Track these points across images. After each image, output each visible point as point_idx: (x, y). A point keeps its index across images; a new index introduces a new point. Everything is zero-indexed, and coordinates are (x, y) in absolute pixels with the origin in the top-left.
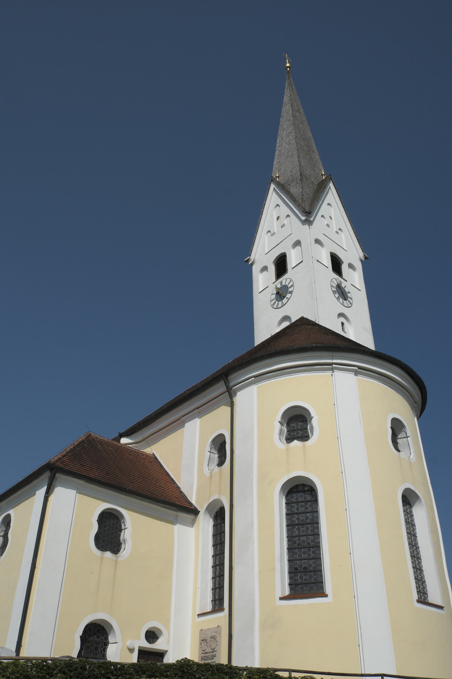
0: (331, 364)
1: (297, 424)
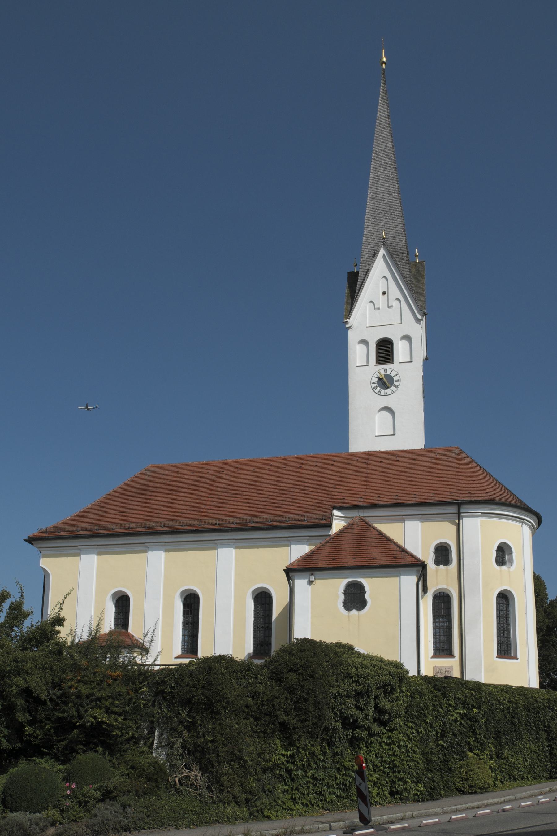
0: (523, 519)
1: (503, 554)
